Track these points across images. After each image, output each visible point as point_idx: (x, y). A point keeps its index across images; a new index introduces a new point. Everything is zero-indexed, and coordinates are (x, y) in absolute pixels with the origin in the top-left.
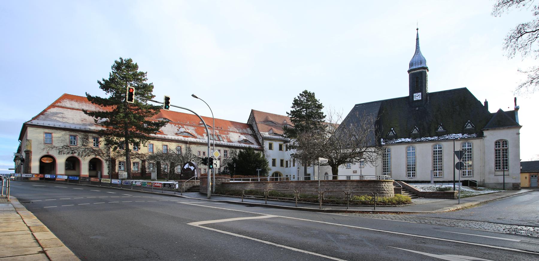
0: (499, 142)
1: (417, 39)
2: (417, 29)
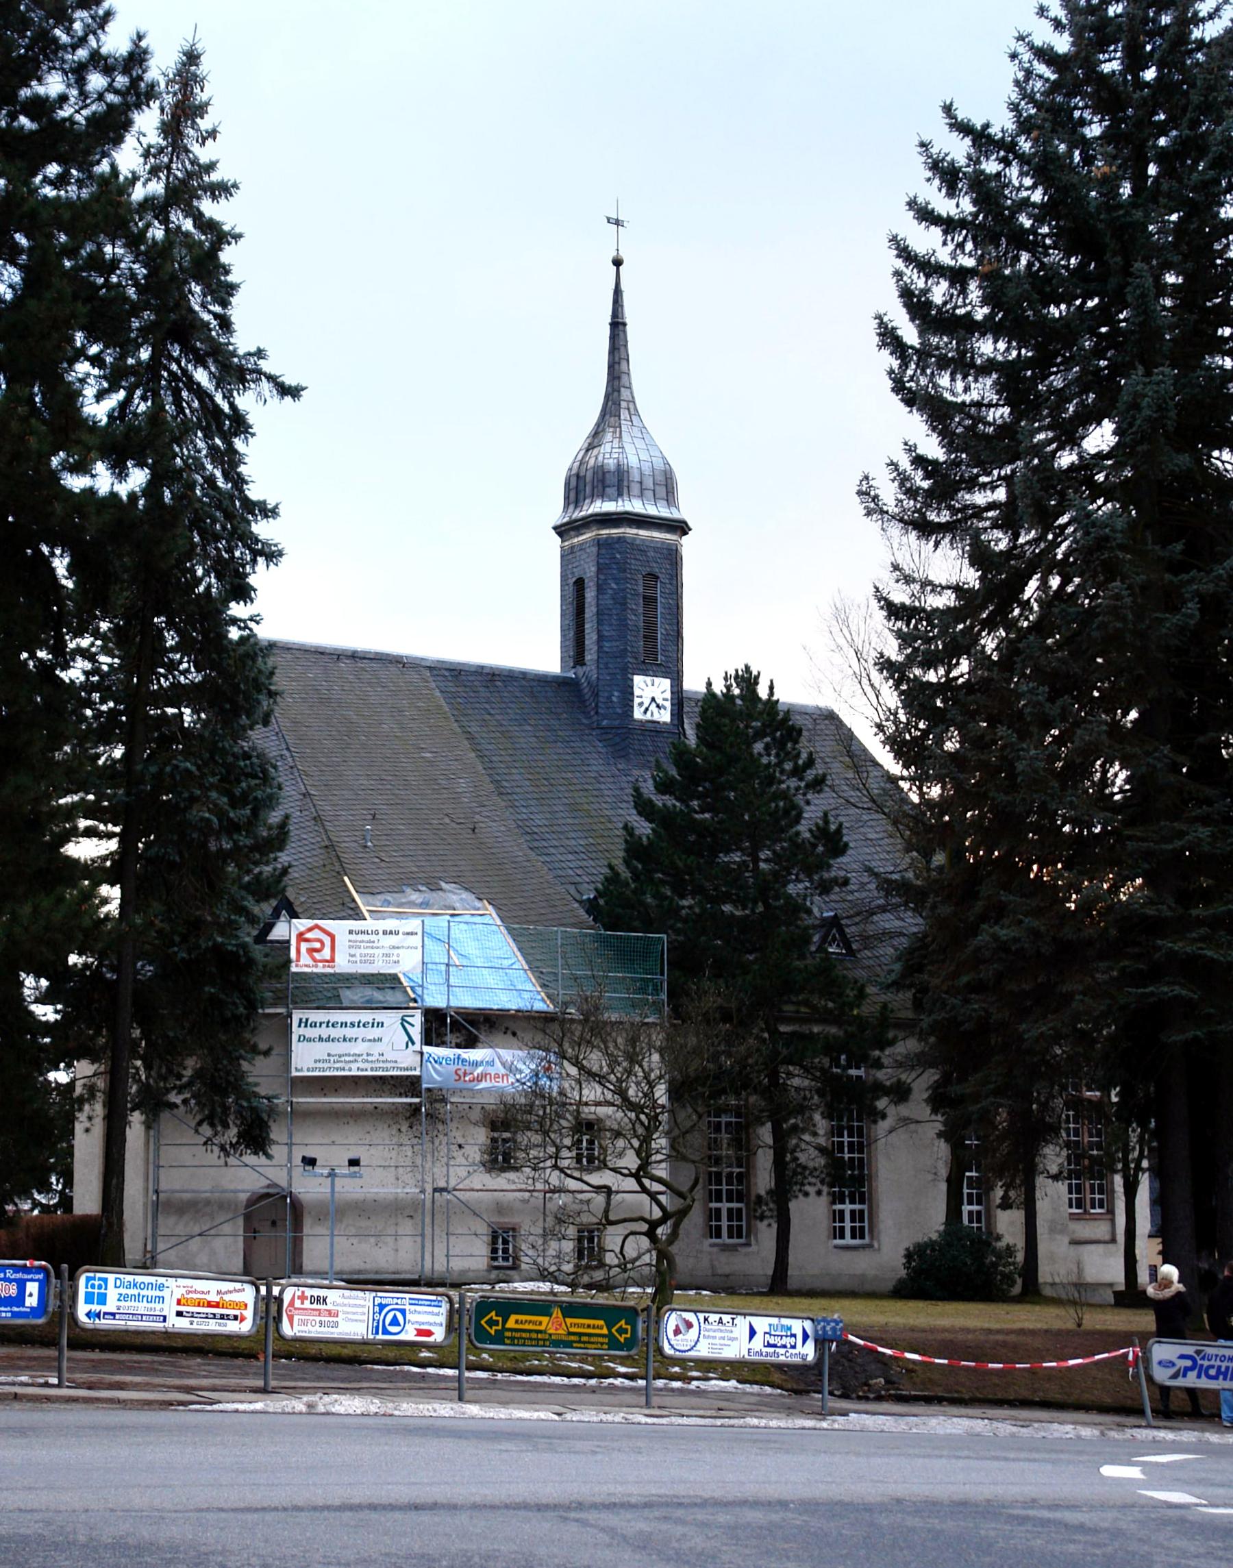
1: (617, 325)
2: (618, 263)
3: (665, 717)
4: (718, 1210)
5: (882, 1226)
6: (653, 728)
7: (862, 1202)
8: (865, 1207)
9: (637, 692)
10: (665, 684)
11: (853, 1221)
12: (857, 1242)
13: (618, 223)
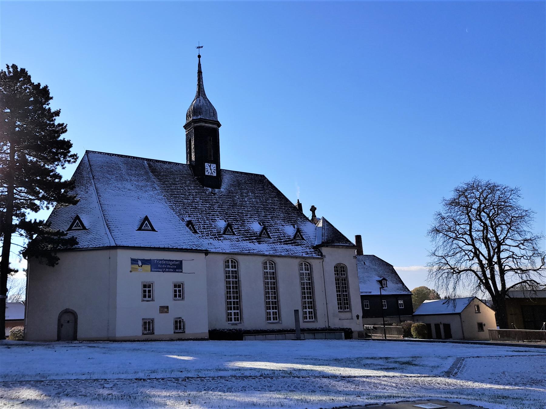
0: (337, 268)
1: (200, 73)
2: (199, 56)
3: (215, 175)
4: (231, 313)
5: (282, 316)
6: (211, 177)
7: (276, 309)
8: (277, 311)
9: (206, 168)
10: (214, 166)
11: (309, 314)
12: (311, 320)
13: (199, 47)
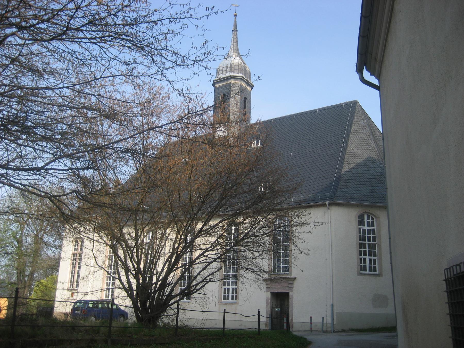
2: (235, 16)
